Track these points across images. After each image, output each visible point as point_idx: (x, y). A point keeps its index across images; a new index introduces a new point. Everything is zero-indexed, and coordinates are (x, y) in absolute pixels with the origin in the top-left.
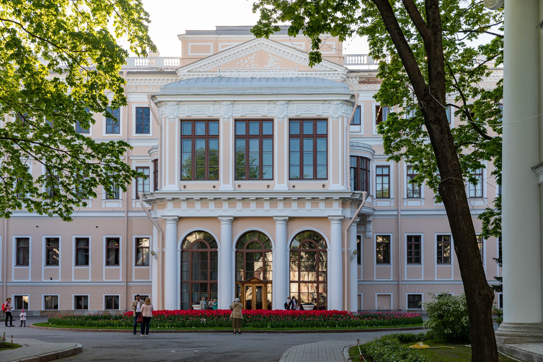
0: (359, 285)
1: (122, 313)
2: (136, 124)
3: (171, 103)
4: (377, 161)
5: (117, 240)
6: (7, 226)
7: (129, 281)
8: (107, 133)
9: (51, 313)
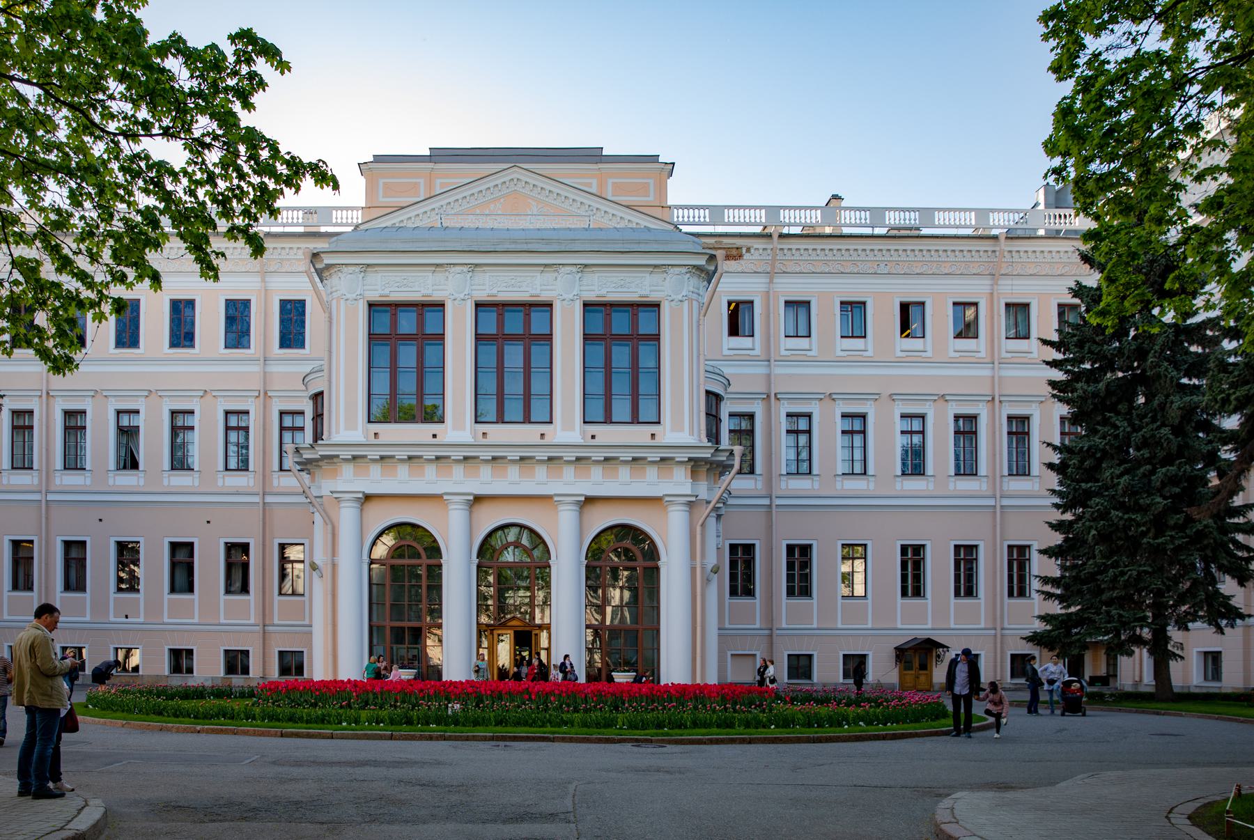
0: (719, 635)
1: (254, 684)
2: (281, 332)
3: (350, 268)
4: (731, 403)
5: (245, 548)
6: (47, 518)
7: (267, 623)
8: (226, 347)
9: (127, 679)
